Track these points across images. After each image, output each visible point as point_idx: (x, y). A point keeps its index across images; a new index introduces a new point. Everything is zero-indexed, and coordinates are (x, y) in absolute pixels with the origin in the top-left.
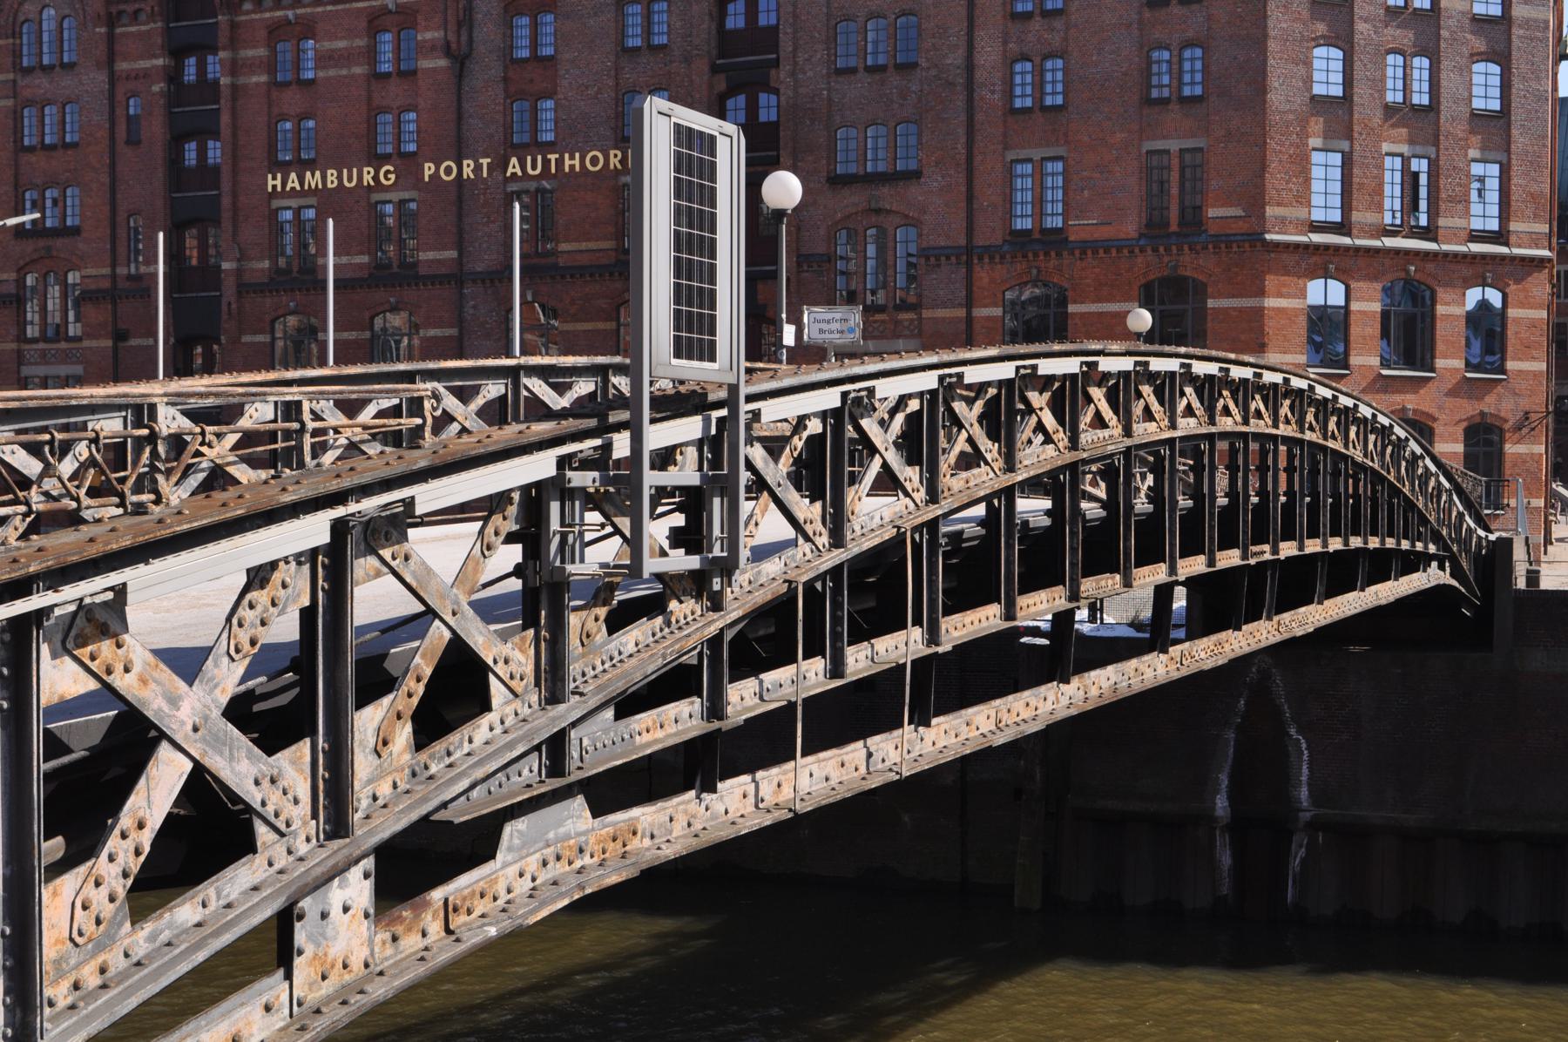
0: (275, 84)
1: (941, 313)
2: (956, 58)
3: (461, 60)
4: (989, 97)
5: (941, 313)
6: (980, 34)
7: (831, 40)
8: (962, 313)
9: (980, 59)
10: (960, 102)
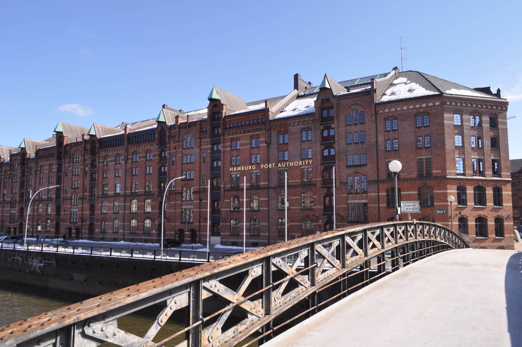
0: (231, 150)
1: (372, 194)
2: (373, 141)
3: (269, 144)
4: (381, 148)
5: (372, 194)
6: (379, 135)
7: (346, 137)
8: (377, 194)
9: (379, 140)
10: (375, 149)
